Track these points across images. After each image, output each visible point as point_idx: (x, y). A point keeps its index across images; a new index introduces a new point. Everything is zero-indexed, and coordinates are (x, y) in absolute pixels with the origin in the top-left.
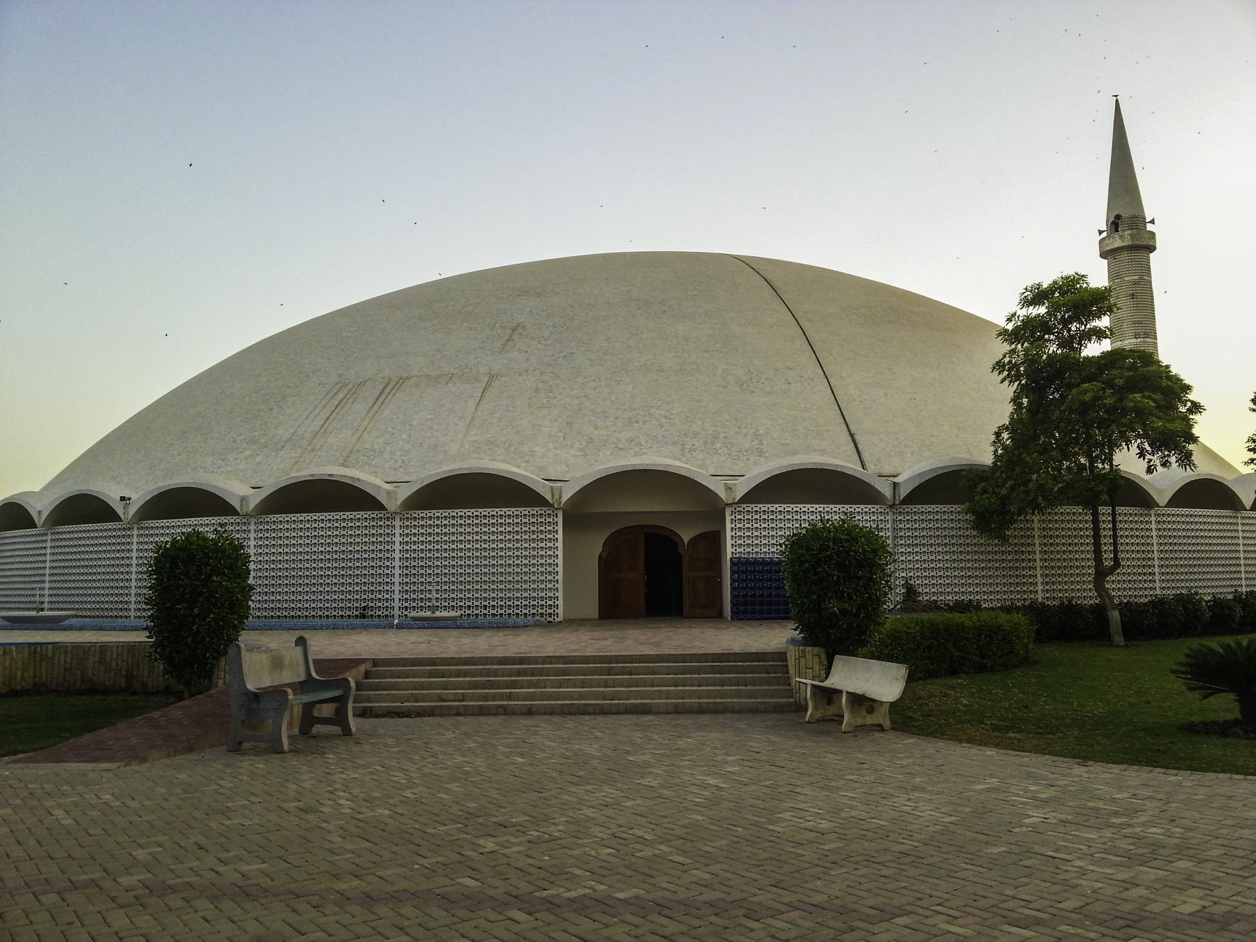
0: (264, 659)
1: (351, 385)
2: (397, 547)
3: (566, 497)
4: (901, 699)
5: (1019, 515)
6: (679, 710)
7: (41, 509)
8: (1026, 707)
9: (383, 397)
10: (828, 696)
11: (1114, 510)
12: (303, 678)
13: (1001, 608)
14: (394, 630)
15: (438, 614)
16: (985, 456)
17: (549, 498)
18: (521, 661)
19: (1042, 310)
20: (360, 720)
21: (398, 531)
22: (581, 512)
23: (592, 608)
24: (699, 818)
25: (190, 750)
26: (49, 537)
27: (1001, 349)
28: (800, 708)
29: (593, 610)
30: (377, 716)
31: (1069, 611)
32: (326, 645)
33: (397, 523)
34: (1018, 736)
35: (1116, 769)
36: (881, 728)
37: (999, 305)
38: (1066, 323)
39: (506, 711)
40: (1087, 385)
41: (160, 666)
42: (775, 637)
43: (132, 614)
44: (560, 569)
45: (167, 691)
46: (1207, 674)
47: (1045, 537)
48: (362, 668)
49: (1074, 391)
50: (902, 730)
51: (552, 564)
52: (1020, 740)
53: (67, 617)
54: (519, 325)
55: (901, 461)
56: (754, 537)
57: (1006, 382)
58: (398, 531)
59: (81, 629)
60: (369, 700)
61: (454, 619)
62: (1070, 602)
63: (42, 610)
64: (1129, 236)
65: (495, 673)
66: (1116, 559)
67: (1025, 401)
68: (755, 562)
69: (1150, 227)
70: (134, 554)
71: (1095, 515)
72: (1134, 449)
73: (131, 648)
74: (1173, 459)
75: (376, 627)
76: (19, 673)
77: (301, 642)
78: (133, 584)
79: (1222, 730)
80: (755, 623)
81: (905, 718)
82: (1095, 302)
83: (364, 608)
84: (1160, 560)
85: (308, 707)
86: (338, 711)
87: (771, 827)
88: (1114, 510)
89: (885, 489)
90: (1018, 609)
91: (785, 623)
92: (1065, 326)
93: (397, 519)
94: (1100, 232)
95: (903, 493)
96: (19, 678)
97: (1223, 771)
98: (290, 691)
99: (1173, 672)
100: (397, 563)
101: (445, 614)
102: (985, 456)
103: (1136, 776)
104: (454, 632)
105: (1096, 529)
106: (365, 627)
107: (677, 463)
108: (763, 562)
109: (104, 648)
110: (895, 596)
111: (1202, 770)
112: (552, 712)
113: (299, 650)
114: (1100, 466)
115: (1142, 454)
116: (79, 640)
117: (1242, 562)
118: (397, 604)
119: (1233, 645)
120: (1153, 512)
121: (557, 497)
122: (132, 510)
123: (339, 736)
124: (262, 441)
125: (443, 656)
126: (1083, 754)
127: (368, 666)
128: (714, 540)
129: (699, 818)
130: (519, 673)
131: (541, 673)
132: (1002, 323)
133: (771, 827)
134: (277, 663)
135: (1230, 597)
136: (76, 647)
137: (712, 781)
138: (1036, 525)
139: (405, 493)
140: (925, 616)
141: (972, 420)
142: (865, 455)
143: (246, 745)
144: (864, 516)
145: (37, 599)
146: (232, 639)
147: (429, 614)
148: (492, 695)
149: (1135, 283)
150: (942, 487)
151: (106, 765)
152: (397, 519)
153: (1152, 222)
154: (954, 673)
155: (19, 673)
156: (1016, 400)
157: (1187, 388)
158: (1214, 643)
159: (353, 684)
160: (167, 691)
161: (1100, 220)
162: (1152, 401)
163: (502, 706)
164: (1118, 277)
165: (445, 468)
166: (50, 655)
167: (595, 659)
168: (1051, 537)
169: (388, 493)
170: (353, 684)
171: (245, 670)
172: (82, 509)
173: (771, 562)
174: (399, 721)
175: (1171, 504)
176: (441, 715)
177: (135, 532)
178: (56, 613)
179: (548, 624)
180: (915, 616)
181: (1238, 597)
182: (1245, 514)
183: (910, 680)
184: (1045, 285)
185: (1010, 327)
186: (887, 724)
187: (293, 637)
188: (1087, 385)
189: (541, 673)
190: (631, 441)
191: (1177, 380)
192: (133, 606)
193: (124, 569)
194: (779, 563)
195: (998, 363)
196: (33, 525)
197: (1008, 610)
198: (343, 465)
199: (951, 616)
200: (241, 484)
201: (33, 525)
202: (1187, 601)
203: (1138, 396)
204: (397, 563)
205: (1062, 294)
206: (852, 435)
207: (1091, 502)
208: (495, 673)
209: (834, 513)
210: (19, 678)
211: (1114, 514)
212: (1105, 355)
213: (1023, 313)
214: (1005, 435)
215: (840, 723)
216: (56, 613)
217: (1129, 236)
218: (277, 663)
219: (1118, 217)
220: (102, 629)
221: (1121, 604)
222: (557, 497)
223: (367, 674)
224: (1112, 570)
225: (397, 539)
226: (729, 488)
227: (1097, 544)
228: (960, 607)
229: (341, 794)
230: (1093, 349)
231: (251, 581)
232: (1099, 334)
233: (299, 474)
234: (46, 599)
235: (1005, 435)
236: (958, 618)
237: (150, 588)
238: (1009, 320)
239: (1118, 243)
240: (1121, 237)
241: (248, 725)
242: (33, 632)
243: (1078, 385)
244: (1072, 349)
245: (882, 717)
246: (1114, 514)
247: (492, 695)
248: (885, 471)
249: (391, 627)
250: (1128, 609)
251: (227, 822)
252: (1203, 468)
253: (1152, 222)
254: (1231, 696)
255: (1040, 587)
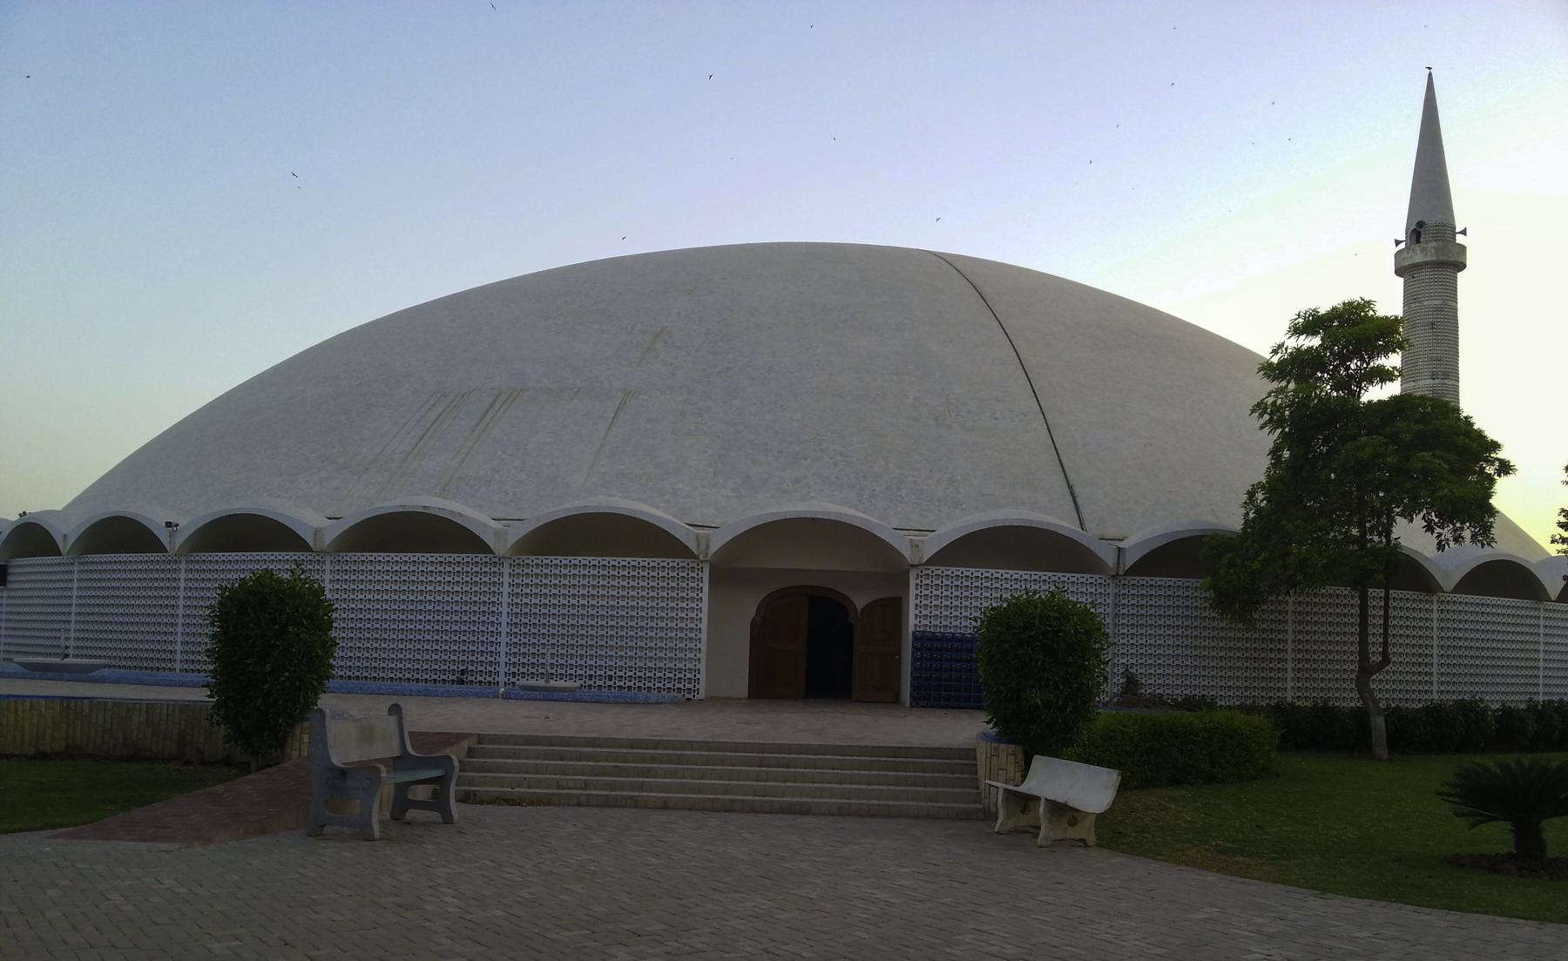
0: (350, 726)
1: (452, 397)
2: (505, 600)
3: (715, 547)
4: (1111, 810)
5: (1270, 593)
6: (843, 812)
7: (67, 533)
8: (1260, 827)
9: (491, 413)
10: (1025, 802)
11: (1387, 594)
12: (397, 753)
13: (1241, 708)
14: (500, 701)
15: (553, 683)
16: (1233, 519)
17: (692, 546)
18: (656, 745)
19: (1316, 342)
20: (462, 805)
21: (506, 580)
22: (730, 568)
23: (740, 683)
24: (864, 935)
25: (263, 832)
26: (76, 568)
27: (1264, 388)
28: (989, 816)
29: (742, 687)
30: (482, 802)
31: (1324, 714)
32: (428, 715)
33: (506, 570)
34: (1248, 860)
35: (1360, 904)
36: (1084, 843)
37: (1262, 328)
38: (1344, 359)
39: (636, 804)
40: (1366, 431)
41: (222, 731)
42: (965, 729)
43: (178, 666)
44: (704, 636)
45: (227, 761)
46: (1480, 798)
47: (1300, 623)
48: (465, 744)
49: (1349, 445)
50: (1109, 847)
51: (703, 634)
52: (1249, 866)
53: (99, 667)
54: (662, 331)
55: (1131, 521)
56: (942, 607)
57: (1267, 430)
58: (506, 580)
59: (117, 681)
60: (472, 782)
61: (572, 690)
62: (1325, 703)
63: (67, 656)
64: (1432, 251)
65: (624, 758)
66: (1385, 654)
67: (1286, 454)
68: (943, 638)
69: (1460, 239)
70: (182, 593)
71: (1364, 598)
72: (1419, 521)
73: (185, 708)
74: (1467, 534)
75: (478, 695)
76: (49, 732)
77: (395, 710)
78: (180, 629)
79: (1491, 865)
80: (941, 712)
81: (1113, 832)
82: (1381, 334)
83: (463, 672)
84: (1450, 659)
85: (402, 788)
86: (435, 794)
87: (948, 950)
88: (1387, 594)
89: (1107, 555)
90: (1260, 709)
91: (976, 713)
92: (1343, 363)
93: (506, 565)
94: (1398, 243)
95: (1129, 561)
96: (48, 738)
97: (1486, 913)
98: (383, 768)
99: (1439, 794)
100: (504, 619)
101: (561, 684)
102: (1233, 519)
103: (1381, 914)
104: (572, 706)
105: (1364, 616)
106: (464, 696)
107: (853, 512)
108: (953, 638)
109: (151, 707)
110: (1112, 687)
111: (1459, 909)
112: (691, 807)
113: (393, 719)
114: (1376, 539)
115: (1429, 528)
116: (116, 696)
117: (1541, 664)
118: (502, 669)
119: (1512, 764)
120: (1435, 598)
121: (703, 546)
122: (180, 539)
123: (435, 823)
124: (341, 460)
125: (562, 734)
126: (1322, 885)
127: (472, 742)
128: (893, 608)
129: (864, 935)
130: (653, 759)
131: (679, 760)
132: (1265, 352)
133: (948, 950)
134: (367, 734)
135: (1523, 706)
136: (118, 703)
137: (882, 896)
138: (1290, 608)
139: (517, 532)
140: (1146, 713)
141: (1223, 474)
142: (1085, 512)
143: (328, 830)
144: (1078, 589)
145: (62, 643)
146: (309, 704)
147: (541, 682)
148: (622, 784)
149: (1438, 309)
150: (1179, 556)
151: (164, 846)
152: (506, 565)
153: (1464, 232)
154: (1177, 782)
155: (49, 732)
156: (1275, 452)
157: (1495, 446)
158: (1491, 762)
159: (456, 764)
160: (227, 761)
161: (1398, 227)
162: (1448, 460)
163: (631, 797)
164: (1416, 300)
165: (576, 504)
166: (87, 711)
167: (745, 747)
168: (1308, 623)
169: (496, 533)
170: (456, 764)
171: (330, 741)
172: (115, 535)
173: (963, 639)
174: (507, 809)
175: (1458, 589)
176: (558, 805)
177: (183, 566)
178: (85, 661)
179: (687, 701)
180: (1134, 712)
181: (1533, 708)
182: (1551, 605)
183: (1123, 788)
184: (1322, 311)
185: (1275, 360)
186: (1092, 839)
187: (385, 703)
188: (1366, 431)
189: (679, 760)
190: (797, 481)
191: (1480, 435)
192: (178, 657)
193: (179, 616)
194: (972, 640)
195: (1258, 405)
196: (57, 552)
197: (1248, 709)
198: (440, 495)
199: (1176, 713)
200: (316, 509)
201: (57, 552)
202: (1469, 711)
203: (1427, 455)
204: (504, 619)
205: (1341, 325)
206: (1070, 487)
207: (1361, 583)
208: (624, 758)
209: (1037, 583)
210: (48, 738)
211: (1387, 599)
212: (1394, 399)
213: (1292, 343)
214: (1260, 496)
215: (1036, 836)
216: (85, 661)
217: (1432, 251)
218: (367, 734)
219: (1421, 224)
220: (141, 682)
221: (1388, 708)
222: (703, 546)
223: (471, 752)
224: (1380, 667)
225: (506, 590)
226: (915, 546)
227: (1363, 635)
228: (1190, 704)
229: (444, 890)
230: (1375, 393)
231: (333, 634)
232: (1384, 375)
233: (387, 504)
234: (72, 643)
235: (1260, 496)
236: (1187, 717)
237: (213, 637)
238: (1275, 352)
239: (1418, 258)
240: (1423, 250)
241: (330, 806)
242: (44, 683)
243: (1354, 438)
244: (1352, 393)
245: (1086, 831)
246: (1387, 599)
247: (622, 784)
248: (1110, 533)
249: (496, 696)
250: (1395, 716)
251: (315, 917)
252: (1503, 548)
253: (1464, 232)
254: (1508, 826)
255: (1290, 684)
